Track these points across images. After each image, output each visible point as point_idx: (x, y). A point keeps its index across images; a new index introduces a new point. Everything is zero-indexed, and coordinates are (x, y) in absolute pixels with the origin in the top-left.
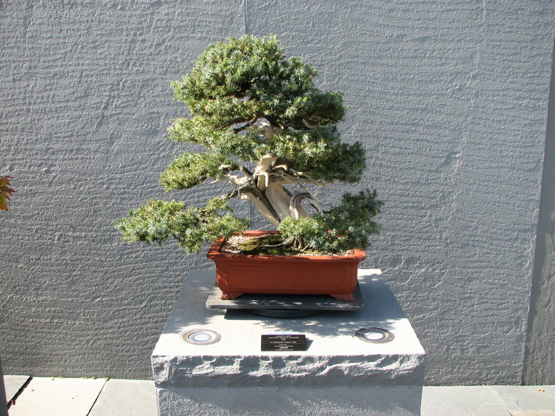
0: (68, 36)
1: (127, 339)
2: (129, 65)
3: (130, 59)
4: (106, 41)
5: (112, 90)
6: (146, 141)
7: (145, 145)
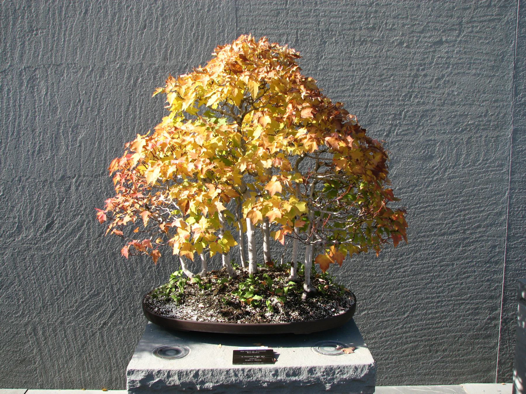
0: (357, 70)
1: (387, 349)
2: (411, 97)
3: (413, 92)
4: (392, 75)
5: (394, 119)
6: (422, 166)
7: (421, 169)
